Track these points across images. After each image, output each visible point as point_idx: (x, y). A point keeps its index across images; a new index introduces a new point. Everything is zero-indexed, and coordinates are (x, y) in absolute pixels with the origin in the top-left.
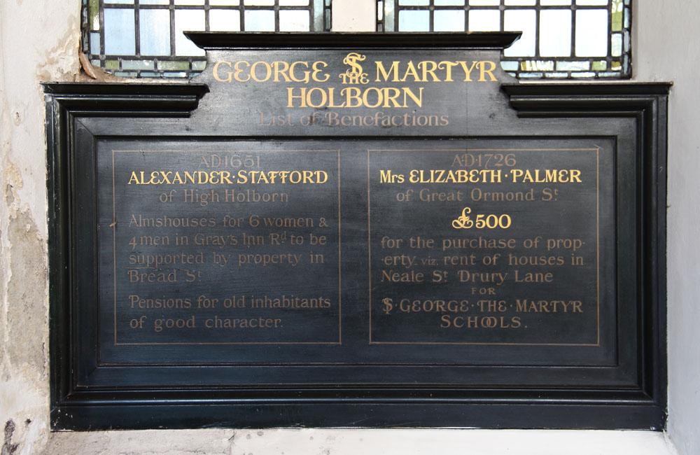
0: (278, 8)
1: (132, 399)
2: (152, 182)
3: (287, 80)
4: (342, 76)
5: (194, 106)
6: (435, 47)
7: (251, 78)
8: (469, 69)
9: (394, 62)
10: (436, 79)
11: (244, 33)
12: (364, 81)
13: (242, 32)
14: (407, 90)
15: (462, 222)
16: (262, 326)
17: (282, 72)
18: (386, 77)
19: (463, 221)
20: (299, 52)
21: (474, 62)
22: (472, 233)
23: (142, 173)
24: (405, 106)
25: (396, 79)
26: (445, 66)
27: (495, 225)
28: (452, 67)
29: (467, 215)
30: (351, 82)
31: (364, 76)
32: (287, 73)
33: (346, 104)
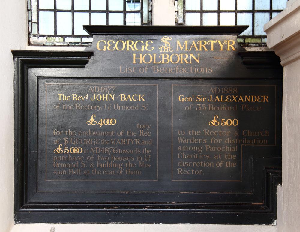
0: (202, 12)
1: (49, 208)
2: (227, 101)
3: (133, 50)
4: (160, 48)
5: (86, 62)
6: (141, 33)
7: (116, 49)
8: (222, 45)
9: (186, 41)
10: (206, 49)
11: (152, 26)
12: (171, 50)
13: (219, 26)
14: (192, 55)
15: (214, 122)
16: (127, 174)
17: (131, 46)
18: (182, 48)
19: (92, 121)
20: (126, 36)
21: (225, 41)
22: (95, 128)
23: (222, 96)
24: (191, 63)
25: (186, 50)
26: (211, 43)
27: (231, 124)
28: (214, 43)
29: (216, 119)
30: (164, 51)
31: (171, 48)
32: (133, 46)
33: (162, 62)
